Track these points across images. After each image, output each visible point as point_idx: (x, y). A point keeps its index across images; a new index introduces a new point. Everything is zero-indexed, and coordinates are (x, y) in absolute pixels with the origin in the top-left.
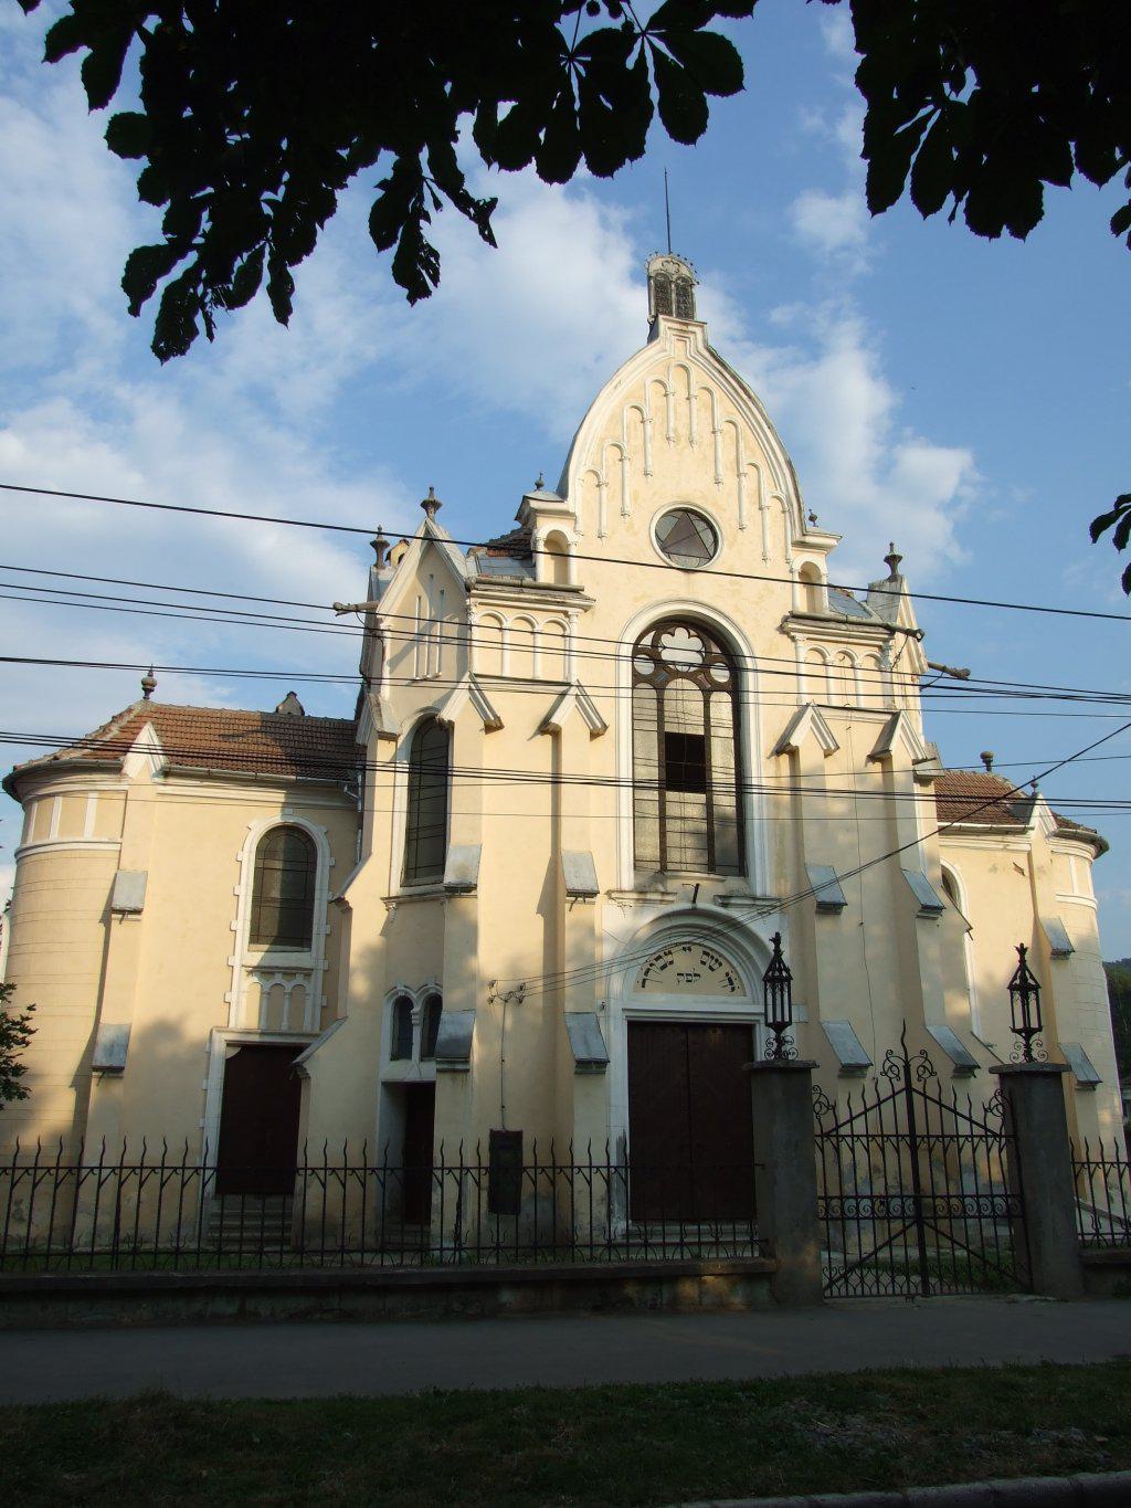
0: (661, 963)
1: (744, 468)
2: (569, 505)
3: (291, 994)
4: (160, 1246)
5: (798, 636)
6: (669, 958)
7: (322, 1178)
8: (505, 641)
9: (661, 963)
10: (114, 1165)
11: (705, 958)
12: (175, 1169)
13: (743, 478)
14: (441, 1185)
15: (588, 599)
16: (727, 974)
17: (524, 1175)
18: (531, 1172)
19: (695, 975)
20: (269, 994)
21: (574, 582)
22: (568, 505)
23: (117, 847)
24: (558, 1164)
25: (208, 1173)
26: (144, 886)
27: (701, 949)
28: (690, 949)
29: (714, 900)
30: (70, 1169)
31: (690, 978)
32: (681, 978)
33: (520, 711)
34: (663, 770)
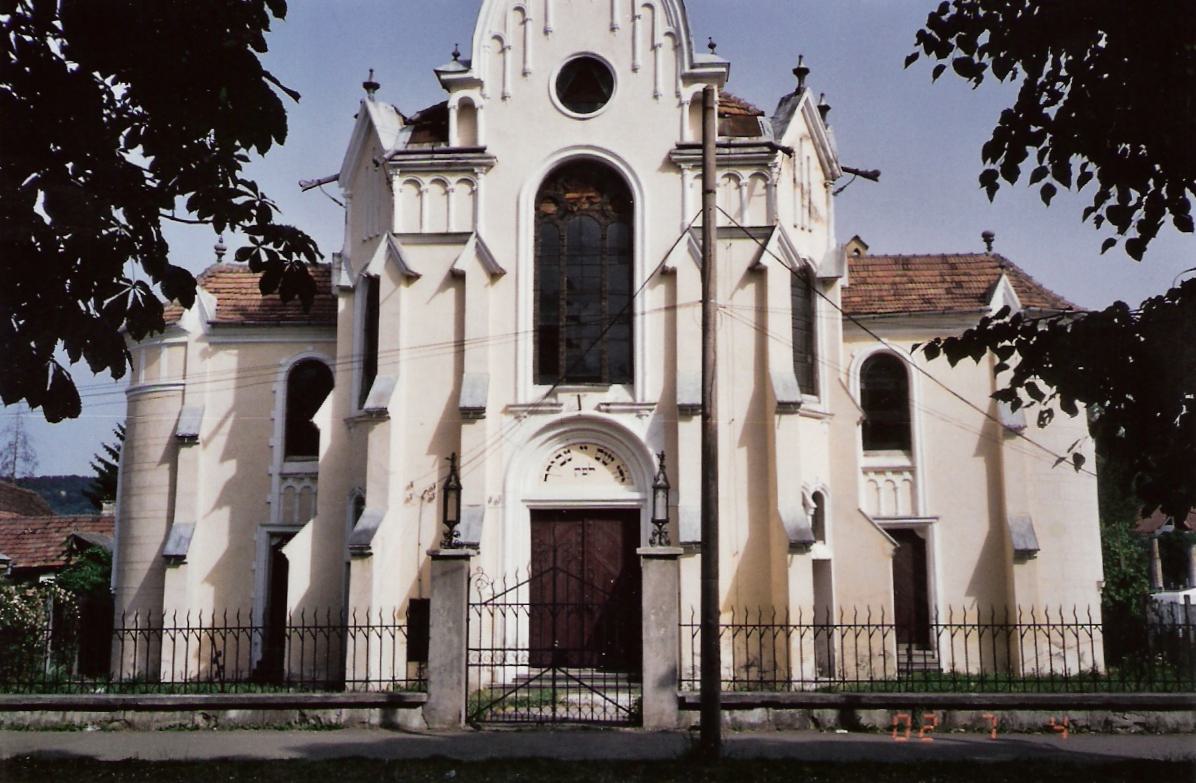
0: (561, 460)
1: (639, 11)
2: (475, 73)
3: (300, 494)
4: (175, 680)
5: (683, 166)
6: (568, 456)
7: (379, 632)
8: (416, 205)
9: (561, 460)
10: (727, 623)
11: (599, 455)
12: (877, 626)
13: (637, 20)
14: (354, 637)
15: (490, 158)
16: (618, 467)
17: (116, 636)
18: (352, 630)
19: (590, 469)
20: (284, 494)
21: (481, 143)
22: (474, 73)
23: (181, 387)
24: (1037, 623)
25: (695, 628)
26: (202, 416)
27: (596, 447)
28: (586, 448)
29: (598, 408)
30: (1001, 626)
31: (585, 472)
32: (577, 472)
33: (429, 262)
34: (539, 293)
